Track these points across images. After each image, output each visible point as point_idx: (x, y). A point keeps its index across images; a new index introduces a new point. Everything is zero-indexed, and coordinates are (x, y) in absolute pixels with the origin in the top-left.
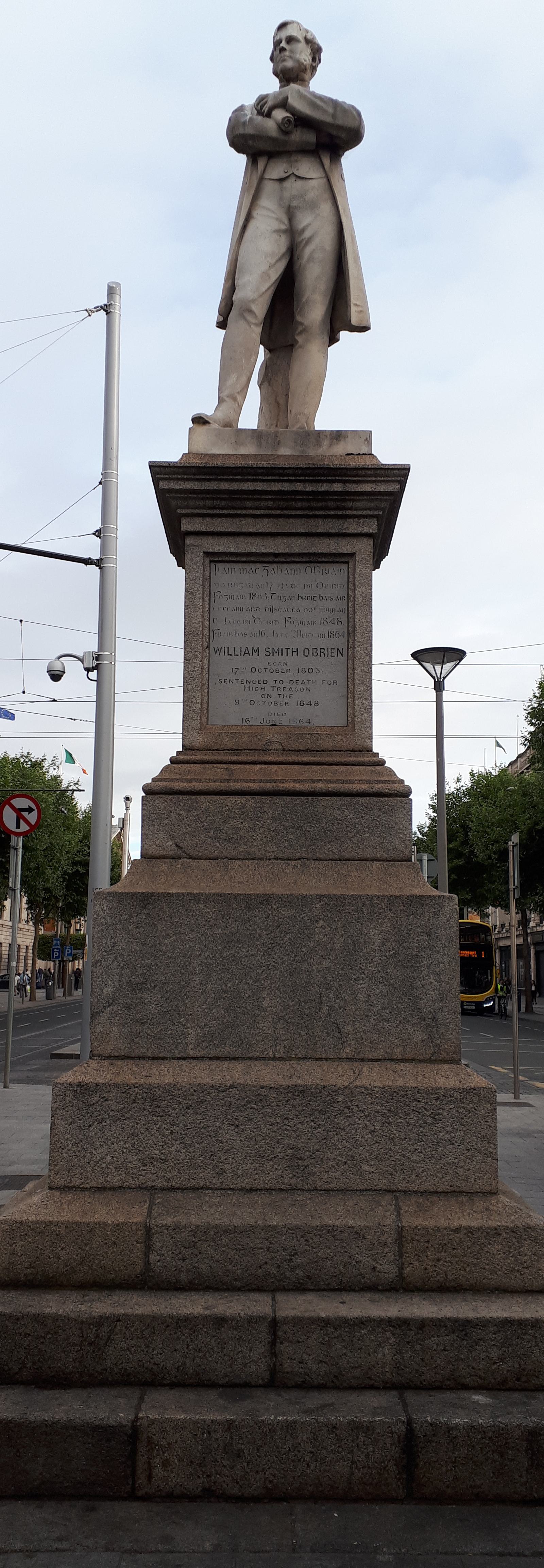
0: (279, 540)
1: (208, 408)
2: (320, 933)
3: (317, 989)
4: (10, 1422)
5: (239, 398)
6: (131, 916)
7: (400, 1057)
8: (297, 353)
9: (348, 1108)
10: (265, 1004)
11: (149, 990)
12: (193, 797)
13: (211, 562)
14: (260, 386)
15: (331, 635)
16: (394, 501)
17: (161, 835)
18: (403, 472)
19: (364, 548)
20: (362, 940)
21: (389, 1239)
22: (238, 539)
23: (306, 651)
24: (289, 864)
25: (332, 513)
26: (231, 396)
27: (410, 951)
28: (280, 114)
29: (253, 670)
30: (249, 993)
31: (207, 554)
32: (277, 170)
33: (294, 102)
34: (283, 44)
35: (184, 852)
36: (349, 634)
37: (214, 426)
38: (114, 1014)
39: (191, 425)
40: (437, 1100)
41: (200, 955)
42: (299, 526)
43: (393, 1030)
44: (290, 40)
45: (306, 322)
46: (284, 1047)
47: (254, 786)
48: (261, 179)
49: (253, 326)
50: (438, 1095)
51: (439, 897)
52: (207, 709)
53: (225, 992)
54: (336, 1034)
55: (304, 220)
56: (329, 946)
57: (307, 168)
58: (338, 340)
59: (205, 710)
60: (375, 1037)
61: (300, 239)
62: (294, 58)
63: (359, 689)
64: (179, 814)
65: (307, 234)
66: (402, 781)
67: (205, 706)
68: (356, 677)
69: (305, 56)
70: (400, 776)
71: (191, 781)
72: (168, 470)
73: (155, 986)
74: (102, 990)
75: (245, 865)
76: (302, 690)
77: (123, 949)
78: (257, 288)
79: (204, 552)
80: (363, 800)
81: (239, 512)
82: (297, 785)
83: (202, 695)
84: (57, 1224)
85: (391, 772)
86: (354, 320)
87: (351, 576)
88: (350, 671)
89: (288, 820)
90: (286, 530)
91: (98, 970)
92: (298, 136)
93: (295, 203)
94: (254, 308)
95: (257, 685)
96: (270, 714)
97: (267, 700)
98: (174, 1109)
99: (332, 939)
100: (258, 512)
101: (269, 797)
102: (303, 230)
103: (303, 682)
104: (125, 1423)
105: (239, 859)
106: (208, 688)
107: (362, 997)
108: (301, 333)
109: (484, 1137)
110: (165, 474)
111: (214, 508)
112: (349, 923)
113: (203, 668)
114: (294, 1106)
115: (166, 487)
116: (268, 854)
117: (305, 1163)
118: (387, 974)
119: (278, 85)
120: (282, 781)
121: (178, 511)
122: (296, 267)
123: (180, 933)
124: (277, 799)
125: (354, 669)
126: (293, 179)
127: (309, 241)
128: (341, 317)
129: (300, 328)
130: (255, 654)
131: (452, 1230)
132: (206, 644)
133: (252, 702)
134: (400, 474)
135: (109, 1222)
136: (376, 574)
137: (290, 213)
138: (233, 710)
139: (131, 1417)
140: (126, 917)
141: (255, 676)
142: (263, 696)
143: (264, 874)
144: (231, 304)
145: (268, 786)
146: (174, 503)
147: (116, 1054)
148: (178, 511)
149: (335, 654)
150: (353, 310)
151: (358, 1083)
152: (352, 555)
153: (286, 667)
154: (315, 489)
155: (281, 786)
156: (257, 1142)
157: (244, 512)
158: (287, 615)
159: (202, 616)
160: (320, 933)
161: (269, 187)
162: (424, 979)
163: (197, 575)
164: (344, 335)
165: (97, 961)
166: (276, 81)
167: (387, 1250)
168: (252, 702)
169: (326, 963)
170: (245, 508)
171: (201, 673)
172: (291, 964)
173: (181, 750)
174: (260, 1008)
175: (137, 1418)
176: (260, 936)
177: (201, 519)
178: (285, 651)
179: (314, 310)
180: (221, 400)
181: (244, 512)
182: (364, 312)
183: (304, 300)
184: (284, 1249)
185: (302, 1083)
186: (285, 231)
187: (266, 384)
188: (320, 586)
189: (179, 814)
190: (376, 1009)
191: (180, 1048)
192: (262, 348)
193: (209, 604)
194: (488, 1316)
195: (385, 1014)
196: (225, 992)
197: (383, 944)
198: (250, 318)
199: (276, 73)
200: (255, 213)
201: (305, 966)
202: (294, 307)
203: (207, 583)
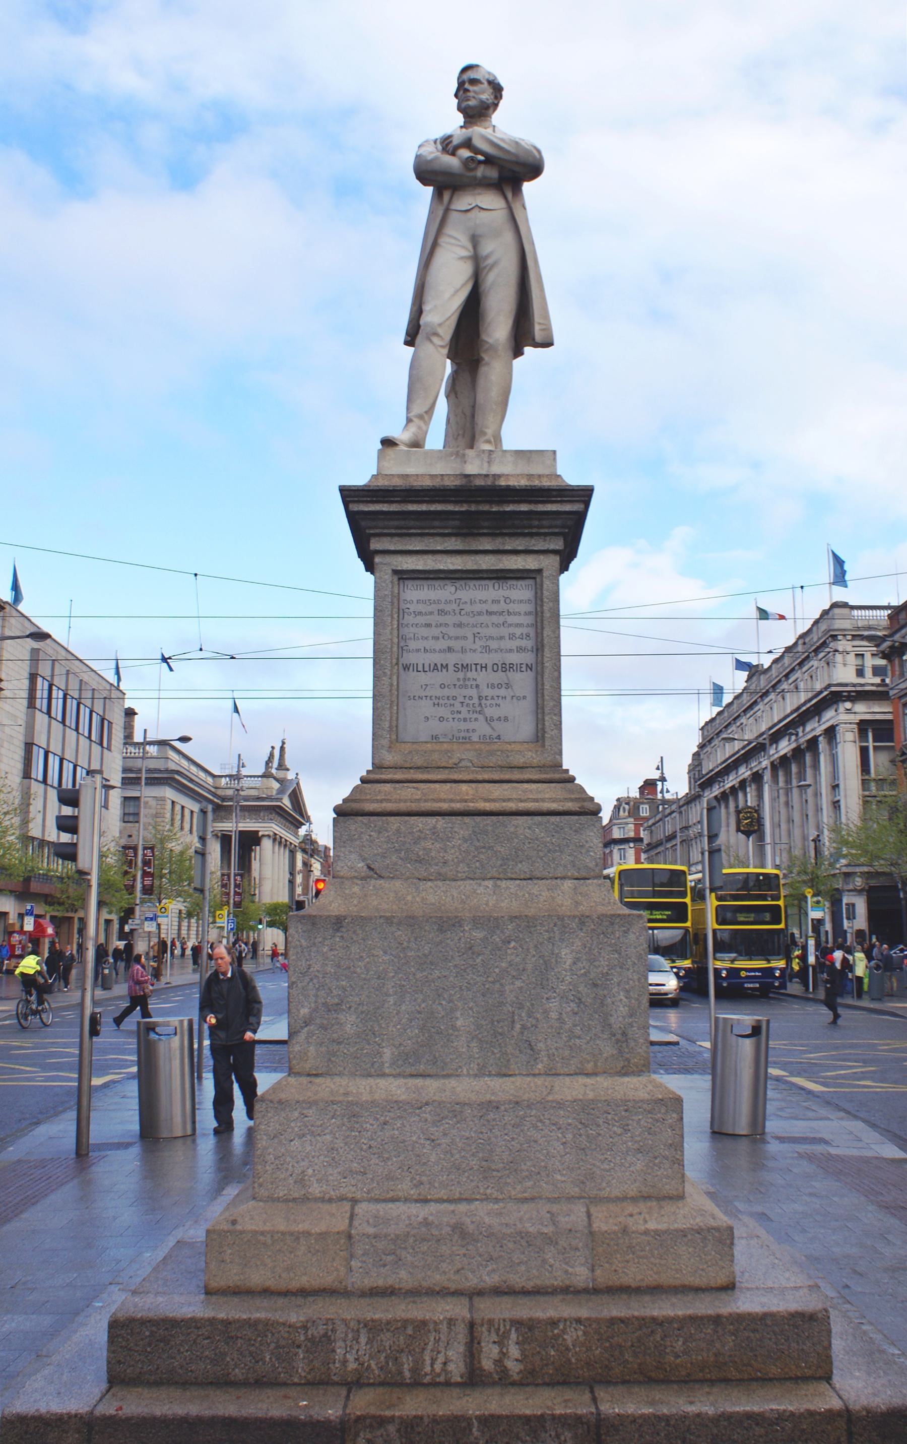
0: (466, 558)
1: (397, 430)
2: (512, 954)
3: (510, 1009)
4: (226, 1418)
5: (426, 417)
6: (325, 939)
7: (590, 1071)
8: (483, 370)
9: (541, 1121)
10: (459, 1023)
11: (344, 1010)
12: (384, 818)
13: (399, 579)
14: (447, 397)
15: (520, 649)
16: (580, 519)
17: (353, 856)
19: (552, 562)
20: (553, 960)
21: (581, 1244)
22: (425, 557)
23: (495, 667)
24: (480, 885)
25: (519, 531)
26: (418, 415)
27: (600, 969)
28: (465, 153)
29: (442, 686)
30: (443, 1013)
31: (395, 572)
32: (464, 201)
33: (478, 143)
34: (467, 86)
35: (376, 873)
36: (537, 650)
37: (403, 448)
38: (310, 1034)
39: (380, 446)
40: (626, 1111)
41: (393, 977)
42: (486, 544)
43: (584, 1046)
44: (474, 82)
45: (490, 341)
46: (478, 1065)
47: (445, 806)
48: (447, 210)
49: (440, 349)
50: (628, 1107)
51: (629, 915)
52: (397, 726)
53: (419, 1012)
54: (529, 1051)
55: (487, 247)
56: (521, 967)
57: (490, 200)
58: (522, 354)
59: (395, 728)
60: (567, 1052)
62: (477, 95)
63: (549, 704)
64: (370, 836)
65: (490, 261)
66: (592, 799)
67: (394, 724)
68: (546, 693)
70: (590, 792)
71: (381, 801)
72: (357, 493)
73: (350, 1007)
74: (299, 1010)
75: (436, 886)
76: (491, 705)
77: (318, 971)
78: (443, 311)
79: (393, 570)
80: (553, 819)
82: (487, 804)
83: (391, 713)
84: (263, 1233)
85: (582, 790)
86: (538, 336)
87: (539, 592)
88: (540, 687)
89: (478, 840)
90: (474, 548)
91: (294, 992)
92: (480, 172)
94: (440, 331)
95: (446, 701)
96: (459, 731)
97: (456, 716)
98: (372, 1125)
99: (524, 959)
101: (459, 818)
102: (487, 257)
103: (493, 698)
104: (332, 1418)
105: (430, 880)
106: (397, 706)
107: (554, 1015)
109: (671, 1145)
111: (401, 528)
112: (541, 944)
113: (391, 685)
114: (488, 1121)
115: (356, 509)
116: (460, 875)
117: (499, 1174)
118: (579, 992)
119: (463, 120)
120: (472, 801)
122: (481, 290)
123: (373, 955)
124: (467, 819)
125: (543, 684)
126: (477, 210)
127: (492, 267)
128: (526, 332)
129: (485, 348)
130: (444, 670)
131: (641, 1234)
132: (394, 661)
133: (441, 719)
134: (585, 495)
135: (313, 1231)
136: (564, 578)
137: (475, 240)
138: (421, 722)
139: (340, 1412)
140: (320, 939)
141: (446, 692)
142: (452, 713)
143: (455, 895)
144: (418, 327)
145: (458, 806)
146: (363, 523)
147: (314, 1072)
148: (367, 531)
149: (524, 669)
150: (537, 328)
151: (550, 1098)
152: (540, 571)
153: (474, 683)
154: (501, 510)
155: (471, 806)
156: (452, 1156)
157: (432, 531)
158: (476, 630)
159: (391, 633)
160: (512, 954)
161: (453, 217)
162: (614, 996)
163: (386, 593)
164: (528, 350)
165: (293, 983)
166: (460, 119)
167: (578, 1254)
168: (441, 719)
169: (518, 983)
170: (434, 528)
171: (390, 691)
172: (484, 985)
173: (371, 768)
174: (454, 1027)
175: (345, 1414)
176: (452, 957)
177: (389, 538)
178: (474, 667)
179: (498, 327)
180: (409, 420)
181: (432, 531)
182: (548, 330)
184: (480, 1256)
185: (496, 1099)
187: (453, 396)
188: (508, 601)
189: (370, 836)
190: (567, 1027)
191: (376, 1065)
192: (449, 361)
193: (398, 621)
194: (672, 1314)
195: (578, 1031)
196: (419, 1012)
197: (574, 963)
198: (436, 340)
199: (460, 109)
201: (497, 986)
202: (480, 331)
203: (395, 600)
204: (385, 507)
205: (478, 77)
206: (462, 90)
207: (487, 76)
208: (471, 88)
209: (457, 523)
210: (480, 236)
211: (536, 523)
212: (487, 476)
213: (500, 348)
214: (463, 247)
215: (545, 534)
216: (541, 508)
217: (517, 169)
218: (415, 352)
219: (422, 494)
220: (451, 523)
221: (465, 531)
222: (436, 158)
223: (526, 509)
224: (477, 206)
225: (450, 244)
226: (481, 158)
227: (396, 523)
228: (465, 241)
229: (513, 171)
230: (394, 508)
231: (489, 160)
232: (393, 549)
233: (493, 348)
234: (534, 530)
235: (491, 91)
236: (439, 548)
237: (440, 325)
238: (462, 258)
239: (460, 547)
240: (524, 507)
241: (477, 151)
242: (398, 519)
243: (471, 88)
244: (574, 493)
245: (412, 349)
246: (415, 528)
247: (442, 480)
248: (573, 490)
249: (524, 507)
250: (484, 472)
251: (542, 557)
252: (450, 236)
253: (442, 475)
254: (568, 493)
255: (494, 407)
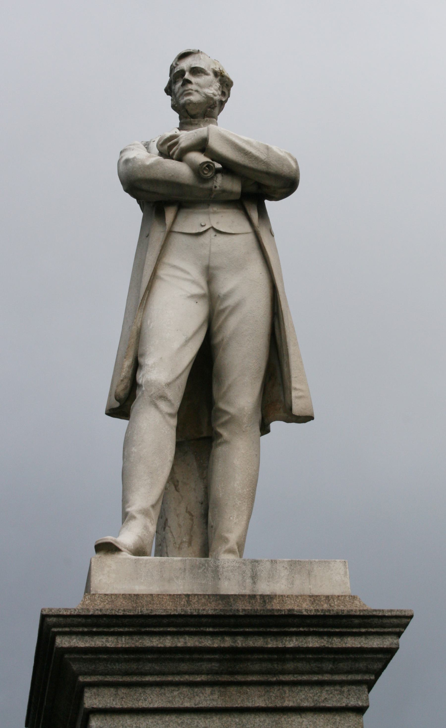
8: (220, 451)
18: (404, 621)
22: (167, 718)
33: (215, 144)
44: (195, 71)
45: (232, 410)
55: (227, 284)
57: (228, 220)
61: (222, 307)
62: (194, 94)
65: (230, 302)
69: (214, 90)
72: (69, 620)
81: (170, 678)
86: (298, 407)
90: (238, 703)
92: (221, 182)
93: (215, 262)
100: (198, 679)
102: (227, 296)
108: (224, 424)
110: (65, 626)
121: (81, 679)
122: (217, 340)
126: (211, 233)
128: (276, 401)
129: (225, 418)
137: (210, 275)
154: (280, 645)
161: (178, 241)
164: (276, 426)
166: (175, 116)
177: (112, 690)
179: (241, 394)
181: (177, 678)
183: (132, 367)
186: (202, 296)
200: (162, 272)
204: (110, 642)
205: (203, 66)
206: (178, 81)
207: (213, 66)
208: (193, 79)
209: (215, 666)
210: (216, 268)
211: (329, 666)
212: (253, 597)
213: (245, 420)
214: (193, 282)
215: (342, 683)
216: (351, 642)
217: (267, 182)
218: (129, 423)
219: (165, 621)
220: (205, 666)
221: (226, 678)
222: (158, 163)
223: (316, 645)
224: (212, 227)
225: (174, 276)
226: (218, 166)
227: (124, 666)
228: (196, 273)
229: (256, 186)
230: (123, 642)
231: (229, 168)
232: (119, 706)
233: (232, 420)
234: (326, 677)
235: (218, 84)
236: (187, 704)
237: (169, 385)
238: (193, 296)
239: (219, 703)
240: (313, 642)
241: (215, 156)
242: (127, 661)
243: (193, 79)
244: (385, 621)
245: (122, 423)
246: (151, 674)
247: (188, 602)
248: (383, 617)
249: (313, 642)
250: (247, 592)
251: (338, 718)
252: (174, 267)
253: (188, 596)
254: (376, 621)
255: (239, 502)
